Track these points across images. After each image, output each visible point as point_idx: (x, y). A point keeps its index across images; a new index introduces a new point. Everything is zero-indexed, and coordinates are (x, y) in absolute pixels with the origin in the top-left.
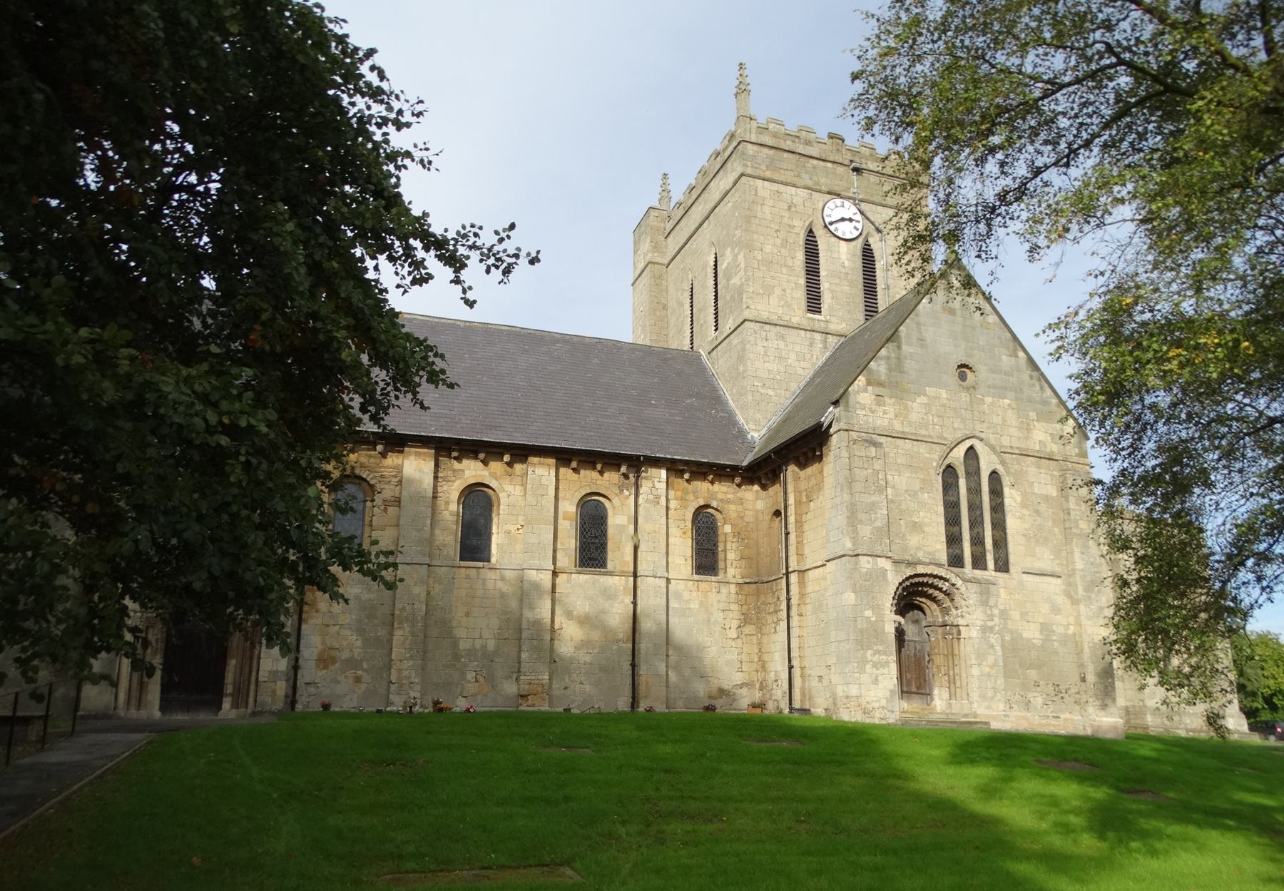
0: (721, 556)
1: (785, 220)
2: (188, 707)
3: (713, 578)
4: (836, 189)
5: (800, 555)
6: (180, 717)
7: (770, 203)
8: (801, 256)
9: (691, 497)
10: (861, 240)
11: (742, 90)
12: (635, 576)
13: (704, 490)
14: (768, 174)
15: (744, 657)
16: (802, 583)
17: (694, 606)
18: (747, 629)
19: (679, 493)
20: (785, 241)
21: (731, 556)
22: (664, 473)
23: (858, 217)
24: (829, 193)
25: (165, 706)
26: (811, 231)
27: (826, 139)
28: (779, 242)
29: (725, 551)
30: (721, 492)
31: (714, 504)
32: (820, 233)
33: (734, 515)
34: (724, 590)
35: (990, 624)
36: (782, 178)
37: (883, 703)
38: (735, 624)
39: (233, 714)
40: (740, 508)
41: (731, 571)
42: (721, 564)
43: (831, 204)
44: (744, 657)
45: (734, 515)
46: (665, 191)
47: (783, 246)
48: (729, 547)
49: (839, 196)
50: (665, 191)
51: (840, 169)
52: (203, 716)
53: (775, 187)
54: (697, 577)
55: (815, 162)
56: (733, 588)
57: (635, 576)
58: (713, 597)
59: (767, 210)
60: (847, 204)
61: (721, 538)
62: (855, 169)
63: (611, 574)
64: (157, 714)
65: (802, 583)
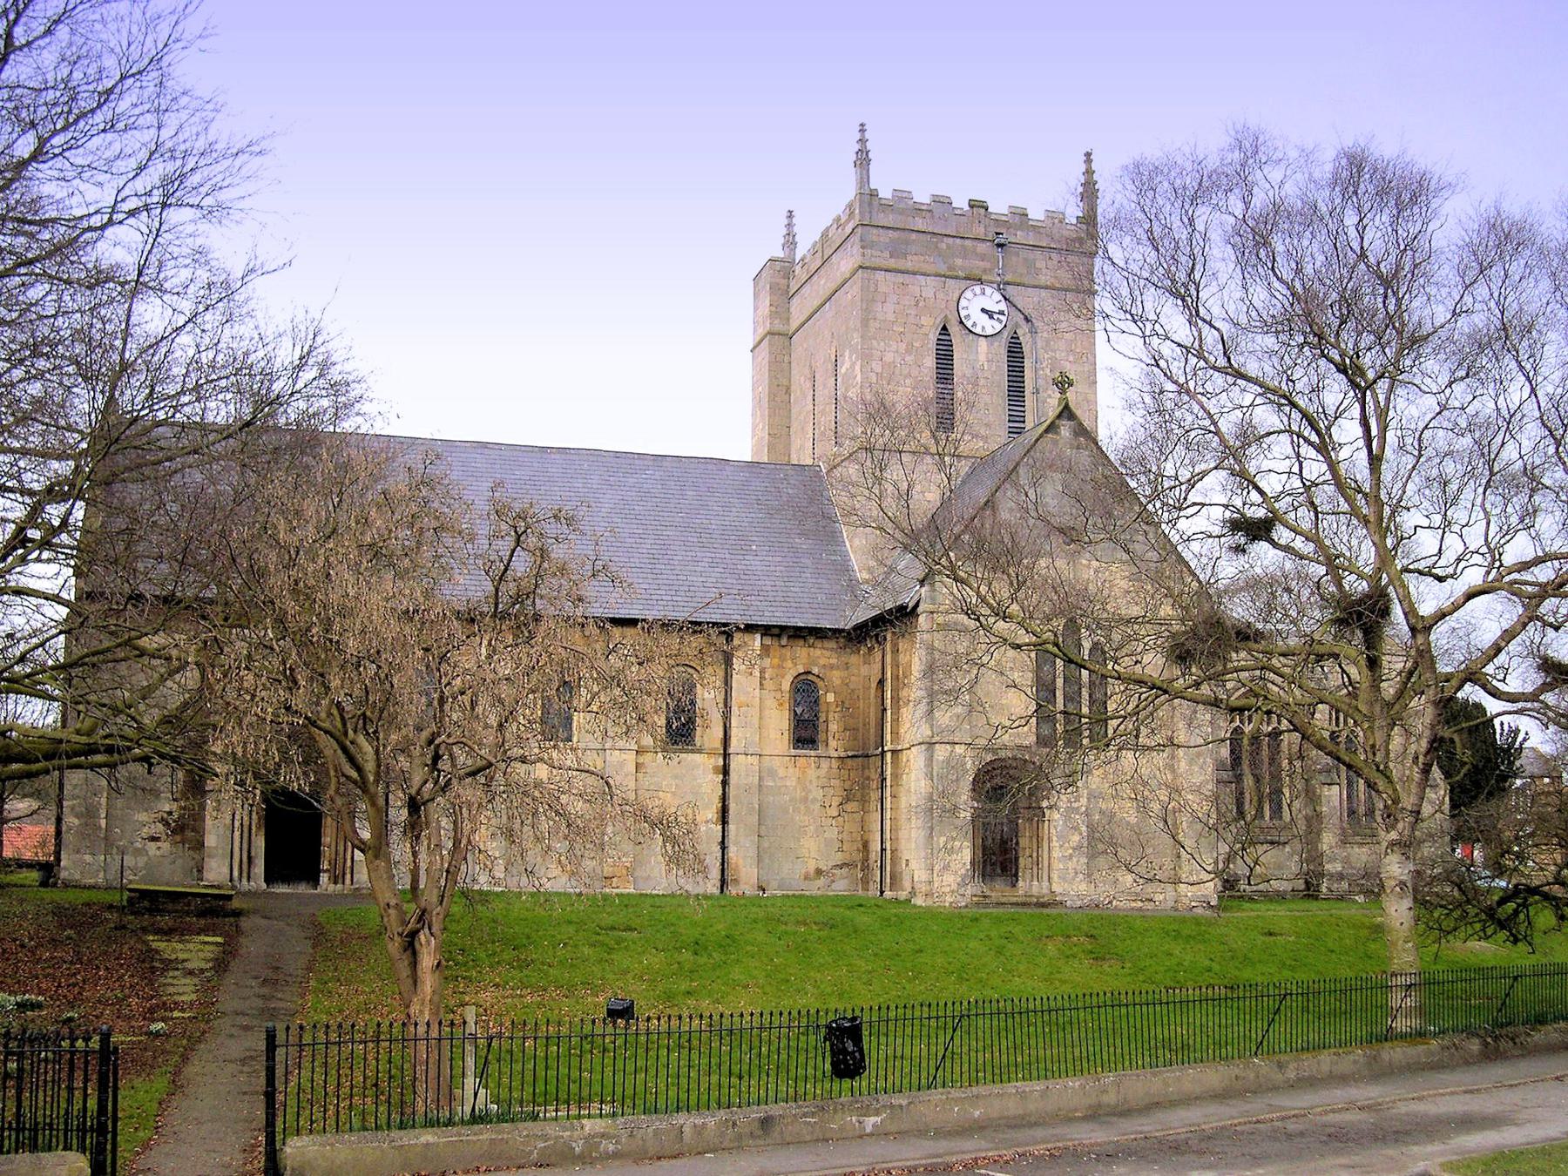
0: (822, 727)
1: (911, 319)
2: (287, 880)
3: (813, 753)
4: (977, 272)
5: (896, 734)
6: (282, 889)
7: (893, 298)
8: (930, 362)
9: (789, 664)
10: (1005, 334)
11: (863, 160)
12: (726, 755)
13: (802, 658)
14: (892, 263)
15: (845, 836)
16: (895, 762)
17: (791, 783)
18: (850, 806)
19: (776, 661)
20: (910, 345)
21: (833, 727)
22: (758, 636)
23: (1003, 306)
24: (967, 278)
25: (269, 879)
26: (944, 328)
27: (966, 208)
28: (903, 346)
29: (826, 721)
30: (819, 657)
31: (815, 670)
32: (954, 329)
33: (837, 682)
34: (825, 764)
35: (1075, 805)
36: (909, 265)
37: (954, 887)
38: (836, 801)
39: (331, 887)
40: (844, 674)
41: (833, 743)
42: (821, 736)
43: (968, 294)
44: (845, 836)
45: (837, 682)
46: (790, 241)
47: (908, 351)
48: (831, 718)
49: (980, 281)
50: (790, 241)
51: (982, 248)
52: (302, 889)
53: (900, 278)
54: (793, 752)
55: (951, 240)
56: (835, 764)
57: (726, 755)
58: (812, 773)
59: (889, 307)
60: (988, 290)
61: (823, 708)
62: (1000, 245)
63: (699, 751)
64: (264, 886)
65: (895, 762)
